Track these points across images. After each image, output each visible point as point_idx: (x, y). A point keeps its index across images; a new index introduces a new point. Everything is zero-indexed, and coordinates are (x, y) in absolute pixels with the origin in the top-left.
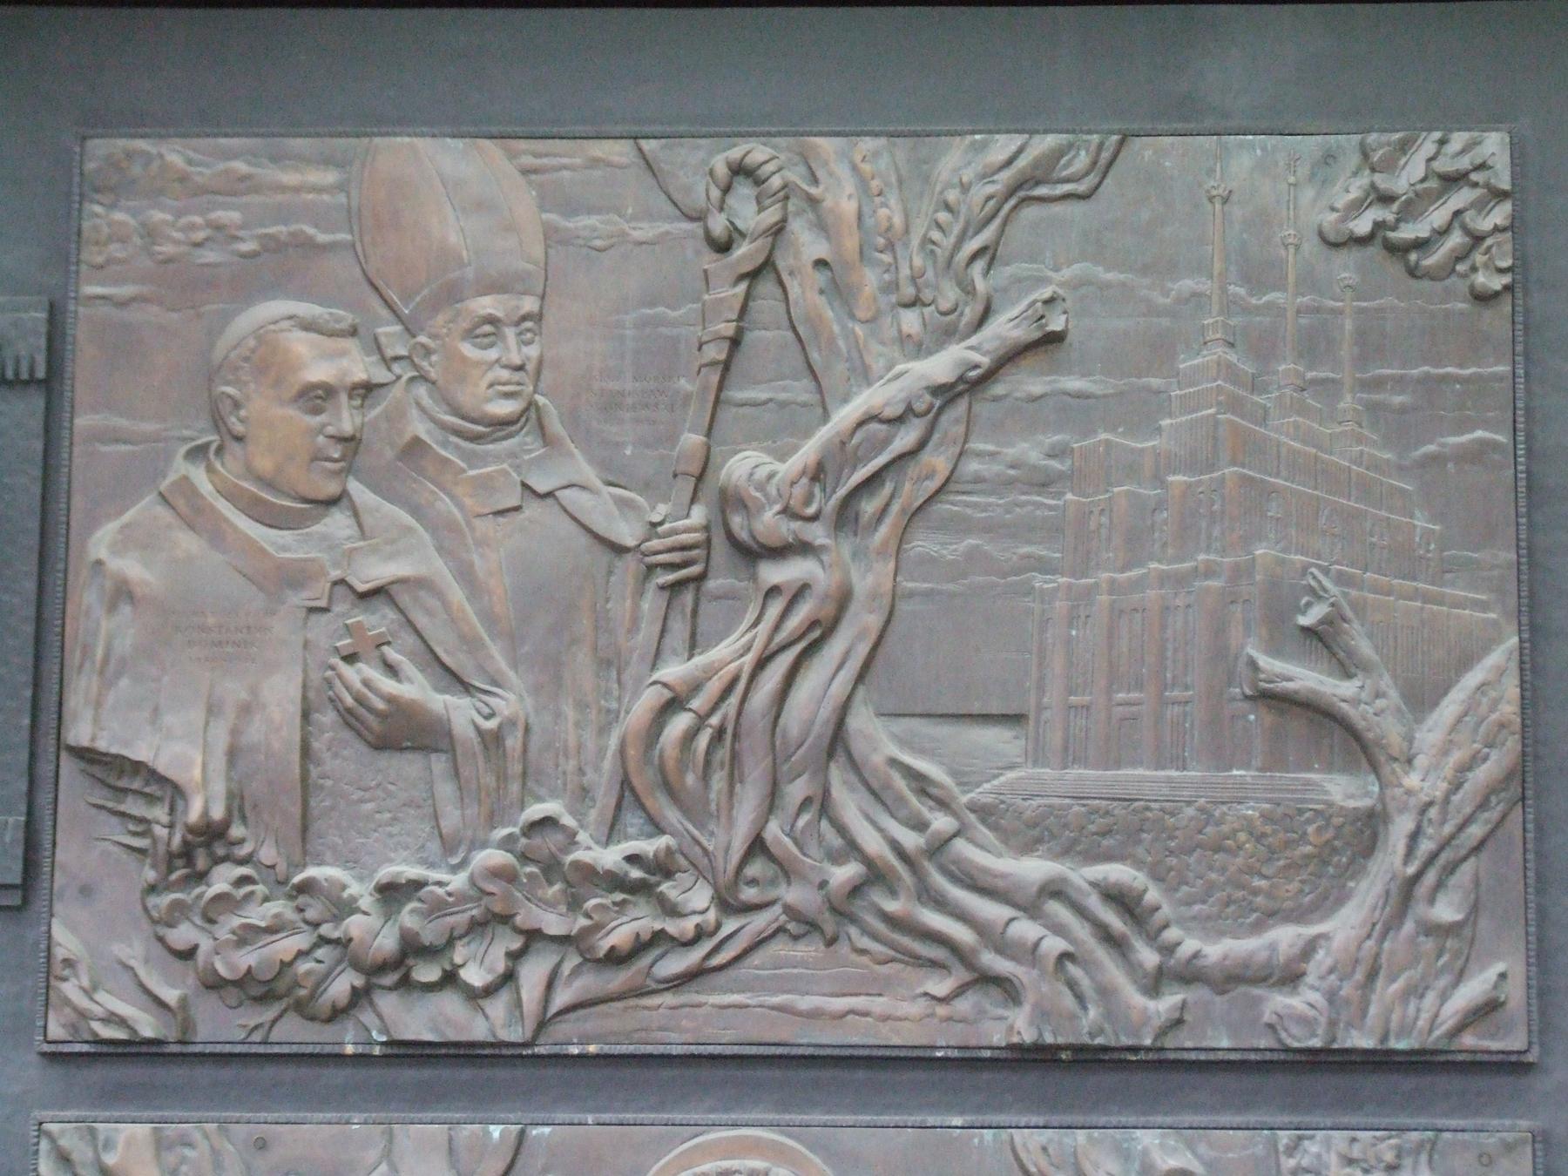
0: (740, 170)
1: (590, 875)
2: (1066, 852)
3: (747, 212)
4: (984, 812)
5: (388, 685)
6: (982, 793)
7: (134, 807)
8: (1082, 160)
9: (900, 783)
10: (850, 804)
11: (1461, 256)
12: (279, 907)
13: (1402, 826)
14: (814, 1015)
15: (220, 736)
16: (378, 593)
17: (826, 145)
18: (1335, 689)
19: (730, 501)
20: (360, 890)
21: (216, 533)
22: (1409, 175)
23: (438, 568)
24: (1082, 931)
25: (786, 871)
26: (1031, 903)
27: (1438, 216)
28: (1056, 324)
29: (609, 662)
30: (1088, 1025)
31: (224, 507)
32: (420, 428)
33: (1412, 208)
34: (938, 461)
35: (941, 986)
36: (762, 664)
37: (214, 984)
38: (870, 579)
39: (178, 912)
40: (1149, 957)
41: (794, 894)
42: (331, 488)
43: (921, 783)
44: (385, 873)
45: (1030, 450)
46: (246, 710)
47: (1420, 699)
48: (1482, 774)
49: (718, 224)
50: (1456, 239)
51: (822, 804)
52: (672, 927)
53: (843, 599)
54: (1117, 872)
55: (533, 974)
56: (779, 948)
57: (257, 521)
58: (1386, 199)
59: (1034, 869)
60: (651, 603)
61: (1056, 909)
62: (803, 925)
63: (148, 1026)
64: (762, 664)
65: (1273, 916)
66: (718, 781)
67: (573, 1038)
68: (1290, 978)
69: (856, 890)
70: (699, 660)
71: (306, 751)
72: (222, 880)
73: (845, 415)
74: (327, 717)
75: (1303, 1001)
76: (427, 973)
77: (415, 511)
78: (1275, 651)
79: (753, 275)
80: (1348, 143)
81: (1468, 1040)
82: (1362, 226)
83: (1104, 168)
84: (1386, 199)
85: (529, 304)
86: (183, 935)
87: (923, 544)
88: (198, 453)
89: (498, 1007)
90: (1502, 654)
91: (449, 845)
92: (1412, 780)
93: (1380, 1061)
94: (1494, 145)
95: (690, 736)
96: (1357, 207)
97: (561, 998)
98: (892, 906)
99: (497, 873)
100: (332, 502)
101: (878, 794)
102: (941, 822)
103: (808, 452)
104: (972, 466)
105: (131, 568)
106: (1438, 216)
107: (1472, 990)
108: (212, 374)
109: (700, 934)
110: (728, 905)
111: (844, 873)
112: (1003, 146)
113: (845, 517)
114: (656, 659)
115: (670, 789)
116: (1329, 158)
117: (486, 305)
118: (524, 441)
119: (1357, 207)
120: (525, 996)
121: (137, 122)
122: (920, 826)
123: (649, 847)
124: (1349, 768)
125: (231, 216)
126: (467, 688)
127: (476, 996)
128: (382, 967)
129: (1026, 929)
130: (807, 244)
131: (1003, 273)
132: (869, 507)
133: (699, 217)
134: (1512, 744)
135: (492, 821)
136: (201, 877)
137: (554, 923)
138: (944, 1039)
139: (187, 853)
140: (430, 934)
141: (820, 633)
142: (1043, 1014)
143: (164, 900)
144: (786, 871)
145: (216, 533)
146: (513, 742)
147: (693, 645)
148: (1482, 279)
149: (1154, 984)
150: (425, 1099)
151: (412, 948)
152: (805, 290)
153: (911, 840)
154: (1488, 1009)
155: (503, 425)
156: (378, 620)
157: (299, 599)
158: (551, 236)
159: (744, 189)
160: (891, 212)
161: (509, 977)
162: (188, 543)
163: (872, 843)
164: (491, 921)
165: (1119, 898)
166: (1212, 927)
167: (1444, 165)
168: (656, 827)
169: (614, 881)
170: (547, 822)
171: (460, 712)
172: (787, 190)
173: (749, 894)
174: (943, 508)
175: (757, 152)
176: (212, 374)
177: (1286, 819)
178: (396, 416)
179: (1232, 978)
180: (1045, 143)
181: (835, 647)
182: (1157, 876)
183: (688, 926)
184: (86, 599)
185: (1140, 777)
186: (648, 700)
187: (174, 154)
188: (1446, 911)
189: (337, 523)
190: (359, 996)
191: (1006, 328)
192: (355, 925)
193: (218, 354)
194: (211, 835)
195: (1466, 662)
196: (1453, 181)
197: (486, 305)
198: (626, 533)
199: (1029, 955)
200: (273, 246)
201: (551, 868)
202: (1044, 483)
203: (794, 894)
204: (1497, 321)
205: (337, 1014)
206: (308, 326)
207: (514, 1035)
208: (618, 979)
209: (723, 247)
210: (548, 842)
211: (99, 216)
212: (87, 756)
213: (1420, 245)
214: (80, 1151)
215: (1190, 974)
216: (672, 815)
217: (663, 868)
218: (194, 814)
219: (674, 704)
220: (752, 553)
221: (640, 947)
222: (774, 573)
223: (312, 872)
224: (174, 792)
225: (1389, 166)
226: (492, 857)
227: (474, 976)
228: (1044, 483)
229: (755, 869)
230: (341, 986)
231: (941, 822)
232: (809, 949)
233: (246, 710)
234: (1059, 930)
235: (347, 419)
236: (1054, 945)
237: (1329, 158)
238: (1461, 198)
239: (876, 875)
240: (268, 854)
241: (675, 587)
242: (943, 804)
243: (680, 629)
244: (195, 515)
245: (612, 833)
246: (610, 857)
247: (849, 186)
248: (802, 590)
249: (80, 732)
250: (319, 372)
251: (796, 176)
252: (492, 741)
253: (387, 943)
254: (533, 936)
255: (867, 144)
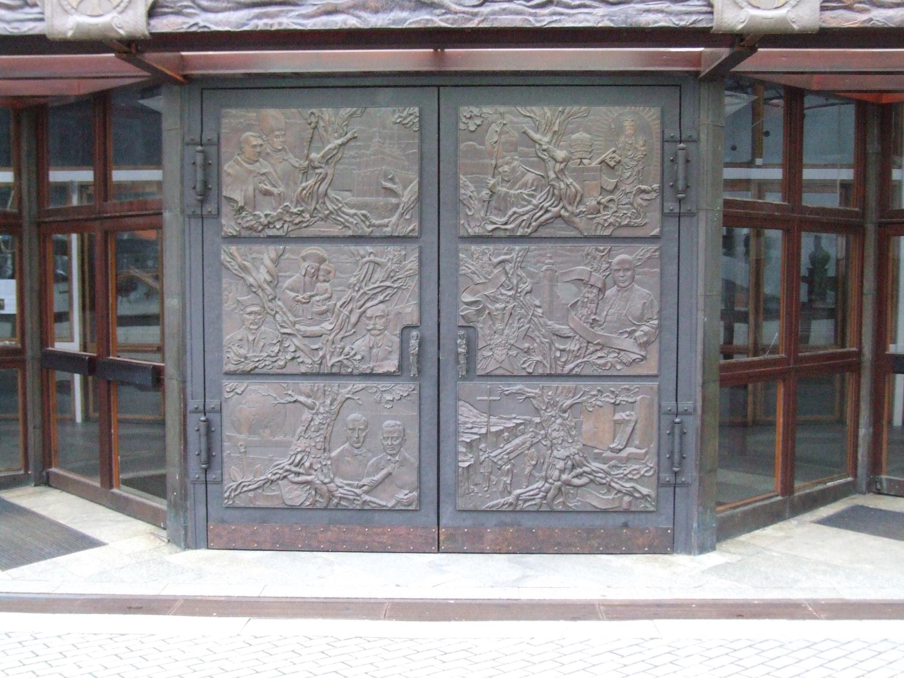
0: (312, 113)
1: (292, 213)
2: (357, 209)
3: (313, 119)
4: (346, 204)
5: (265, 187)
6: (346, 201)
7: (232, 204)
8: (359, 112)
9: (334, 200)
10: (328, 203)
11: (412, 125)
12: (252, 217)
13: (402, 205)
14: (324, 231)
15: (243, 193)
16: (264, 174)
17: (324, 109)
18: (393, 186)
19: (311, 161)
20: (262, 215)
21: (241, 165)
22: (405, 113)
23: (272, 170)
24: (359, 220)
25: (319, 212)
26: (352, 216)
27: (409, 119)
28: (356, 135)
29: (295, 183)
30: (360, 232)
31: (242, 162)
32: (268, 150)
33: (405, 118)
34: (340, 155)
35: (340, 227)
36: (316, 183)
37: (243, 228)
38: (330, 172)
39: (238, 218)
40: (368, 223)
41: (320, 215)
42: (257, 159)
43: (337, 200)
44: (266, 213)
45: (352, 153)
46: (246, 190)
47: (405, 188)
48: (413, 198)
49: (309, 121)
50: (411, 123)
51: (324, 203)
52: (304, 220)
53: (326, 174)
54: (364, 212)
55: (286, 226)
56: (318, 222)
57: (897, 496)
58: (401, 117)
59: (352, 211)
60: (301, 176)
61: (356, 217)
62: (322, 219)
63: (235, 234)
64: (316, 183)
65: (384, 218)
66: (310, 200)
67: (292, 235)
68: (387, 226)
69: (328, 215)
70: (308, 183)
71: (255, 197)
72: (244, 214)
73: (327, 148)
74: (257, 191)
75: (388, 229)
76: (271, 226)
77: (269, 162)
78: (385, 181)
79: (314, 128)
80: (397, 109)
81: (410, 234)
82: (398, 121)
83: (363, 113)
84: (401, 117)
85: (283, 133)
86: (239, 221)
87: (338, 166)
88: (238, 154)
89: (281, 231)
90: (416, 182)
91: (274, 209)
92: (403, 199)
93: (398, 237)
94: (417, 109)
95: (306, 194)
96: (398, 118)
97: (289, 229)
98: (333, 217)
99: (280, 213)
100: (257, 161)
101: (332, 202)
102: (340, 205)
103: (322, 154)
104: (344, 155)
105: (230, 171)
106: (409, 119)
107: (411, 227)
108: (240, 143)
109: (308, 221)
110: (311, 216)
111: (327, 212)
112: (349, 109)
113: (327, 163)
114: (301, 183)
115: (304, 201)
116: (394, 111)
117: (277, 133)
118: (283, 152)
119: (398, 118)
120: (611, 230)
121: (229, 106)
122: (337, 206)
123: (301, 209)
124: (395, 197)
125: (242, 120)
126: (276, 187)
127: (278, 229)
128: (266, 225)
129: (351, 220)
130: (322, 124)
131: (349, 128)
132: (330, 161)
133: (307, 120)
134: (417, 194)
135: (280, 205)
136: (241, 213)
137: (288, 219)
138: (341, 235)
139: (239, 210)
140: (272, 221)
141: (323, 179)
142: (354, 231)
143: (236, 217)
144: (319, 212)
145: (241, 165)
146: (282, 195)
147: (307, 181)
148: (414, 129)
149: (369, 227)
150: (273, 243)
151: (269, 223)
152: (321, 130)
153: (336, 208)
154: (413, 230)
155: (280, 150)
156: (263, 178)
157: (253, 175)
158: (286, 123)
159: (313, 116)
160: (333, 119)
161: (282, 227)
162: (237, 167)
163: (331, 208)
164: (279, 220)
165: (364, 215)
166: (376, 219)
167: (410, 112)
168: (302, 206)
169: (296, 214)
170: (287, 206)
171: (275, 191)
172: (319, 116)
173: (314, 215)
174: (342, 161)
175: (314, 110)
176: (240, 143)
177: (386, 205)
178: (266, 149)
179: (380, 226)
180: (354, 109)
181: (325, 181)
182: (369, 212)
183: (306, 220)
184: (224, 175)
185: (367, 199)
186: (300, 189)
187: (234, 111)
188: (408, 217)
189: (258, 164)
190: (263, 229)
191: (349, 136)
192: (262, 220)
193: (242, 139)
194: (242, 209)
195: (411, 183)
196: (411, 114)
197: (277, 133)
198: (297, 165)
199: (352, 223)
200: (249, 125)
201: (288, 212)
202: (354, 158)
203: (320, 215)
204: (417, 134)
205: (260, 232)
206: (254, 136)
207: (284, 234)
208: (298, 227)
209: (310, 124)
210: (287, 208)
211: (225, 121)
212: (225, 197)
213: (407, 124)
214: (227, 250)
215: (374, 226)
216: (304, 205)
217: (302, 211)
218: (240, 205)
219: (304, 189)
220: (315, 168)
221: (300, 223)
222: (318, 171)
223: (256, 213)
224: (237, 202)
225: (402, 112)
226: (279, 210)
227: (278, 227)
228: (354, 158)
229: (315, 212)
230: (260, 228)
231: (340, 205)
232: (323, 223)
233: (246, 190)
234: (355, 220)
235: (258, 149)
236: (355, 222)
237: (394, 111)
238: (412, 117)
239: (331, 213)
240: (250, 210)
241: (304, 173)
242: (340, 203)
243: (304, 179)
244: (238, 163)
245: (296, 207)
246: (295, 210)
247: (327, 115)
248: (321, 174)
249: (224, 194)
250: (255, 143)
251: (320, 114)
252: (279, 194)
253: (266, 222)
254: (285, 221)
255: (330, 109)
